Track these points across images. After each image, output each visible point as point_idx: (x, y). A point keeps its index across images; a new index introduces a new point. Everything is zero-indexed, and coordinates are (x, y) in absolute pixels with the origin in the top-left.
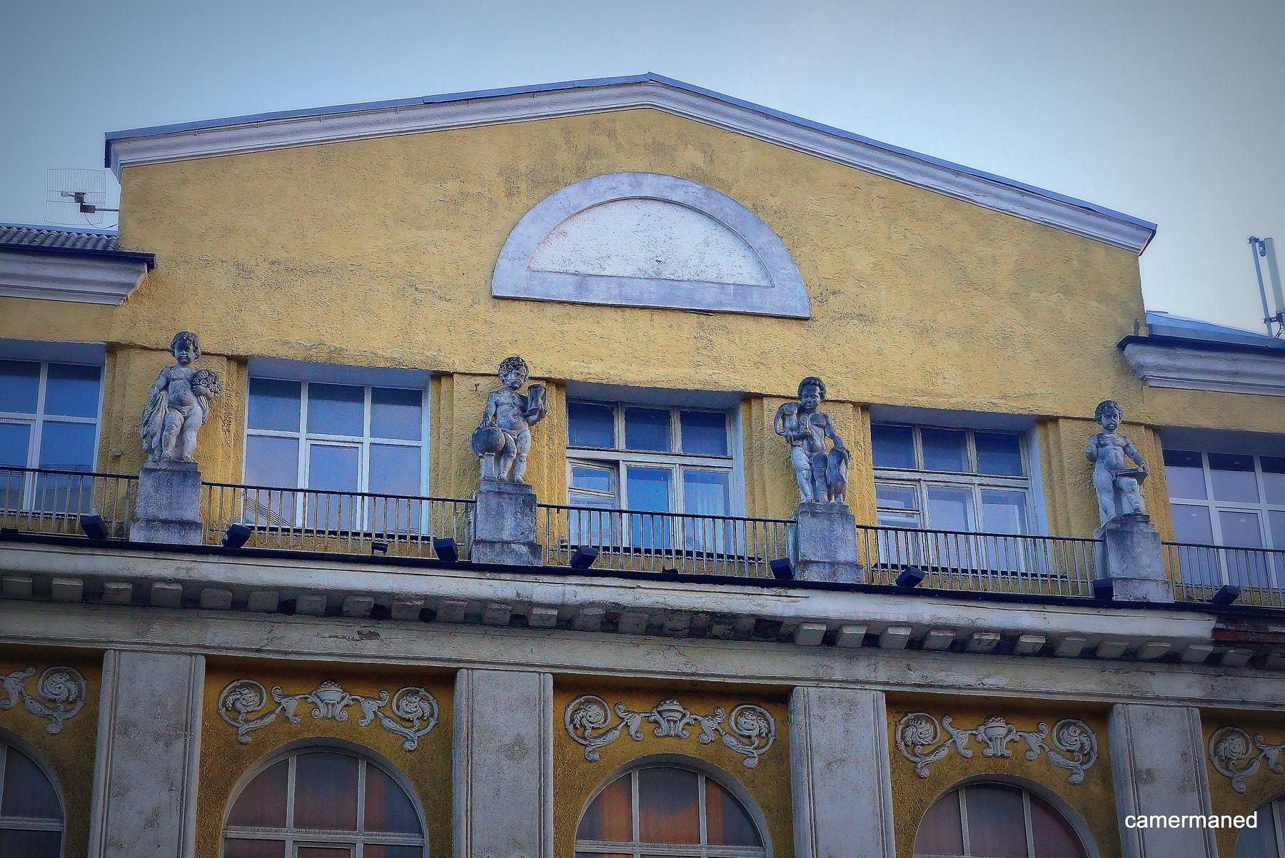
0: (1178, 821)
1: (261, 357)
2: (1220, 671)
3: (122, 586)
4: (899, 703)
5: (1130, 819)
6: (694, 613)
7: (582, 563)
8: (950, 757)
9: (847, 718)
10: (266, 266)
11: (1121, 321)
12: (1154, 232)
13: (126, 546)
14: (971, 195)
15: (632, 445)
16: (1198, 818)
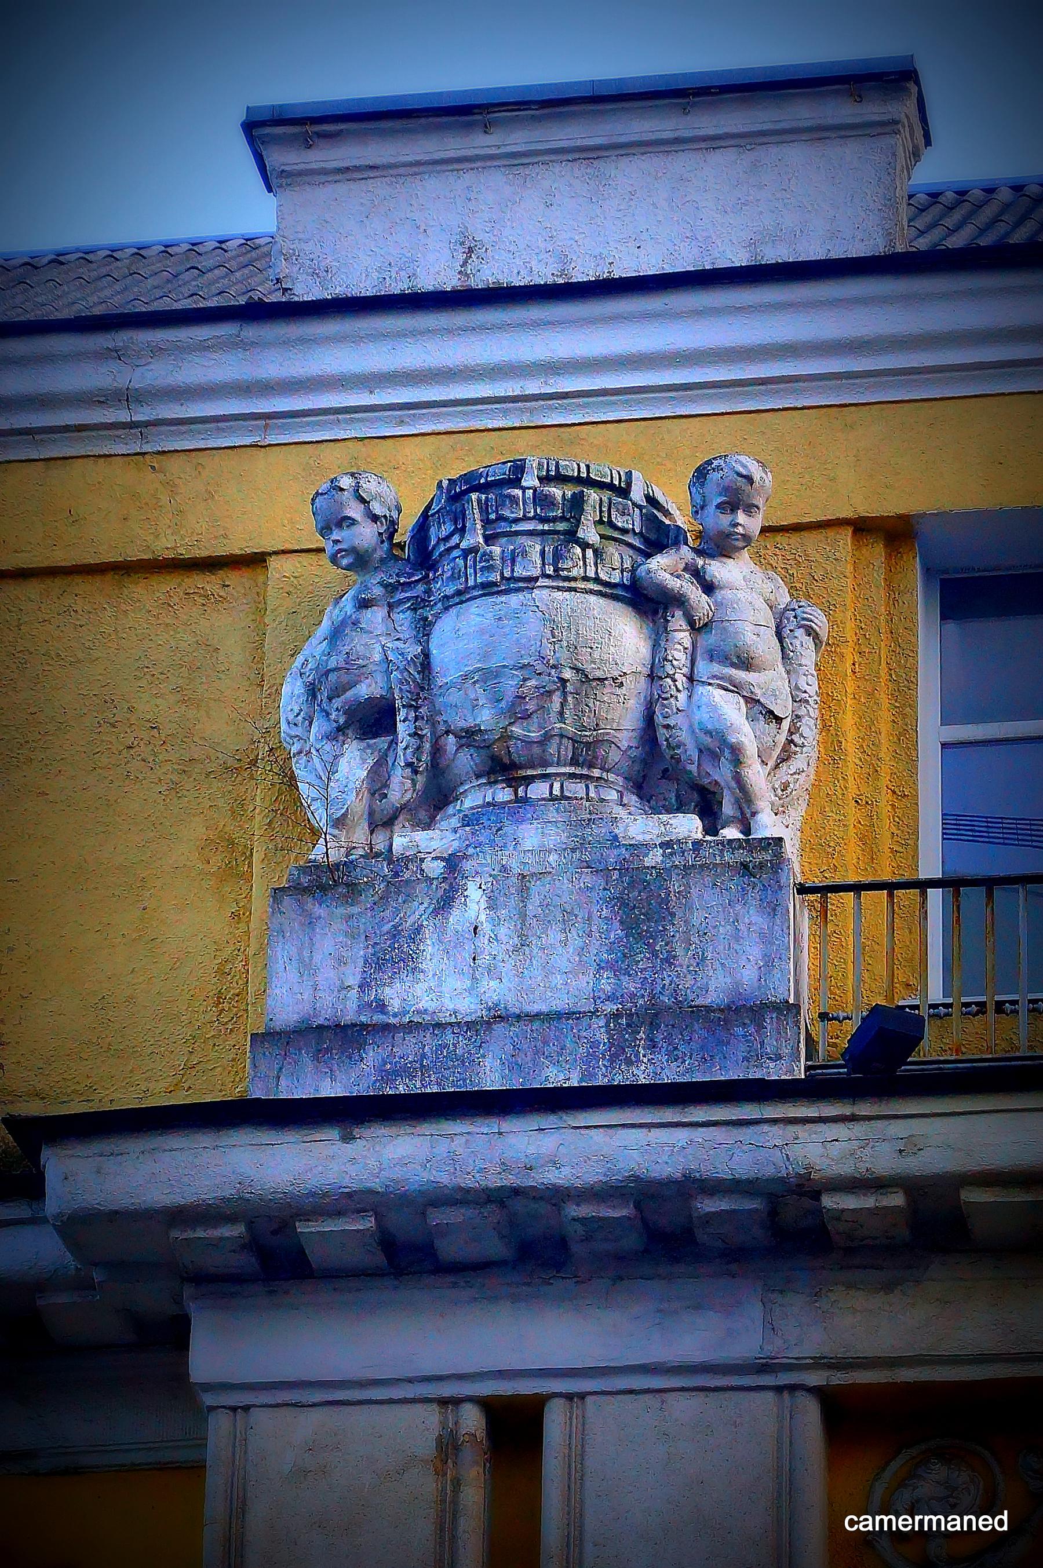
0: (910, 1522)
5: (851, 1520)
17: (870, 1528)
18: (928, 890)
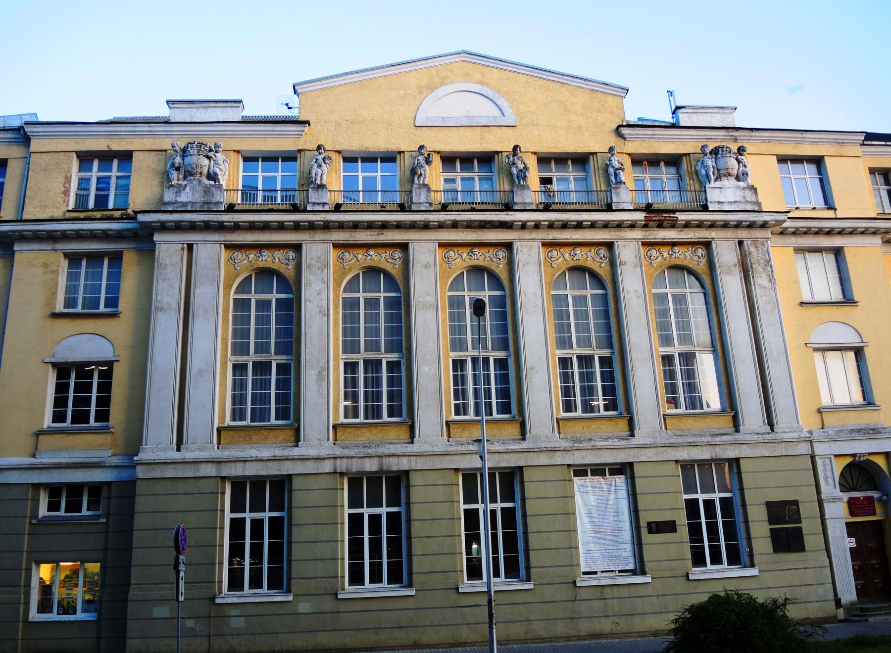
1: (345, 150)
2: (648, 229)
3: (305, 224)
4: (548, 245)
6: (480, 221)
7: (444, 208)
8: (562, 261)
9: (529, 251)
10: (344, 122)
11: (617, 120)
12: (628, 90)
13: (305, 211)
14: (569, 82)
15: (462, 170)
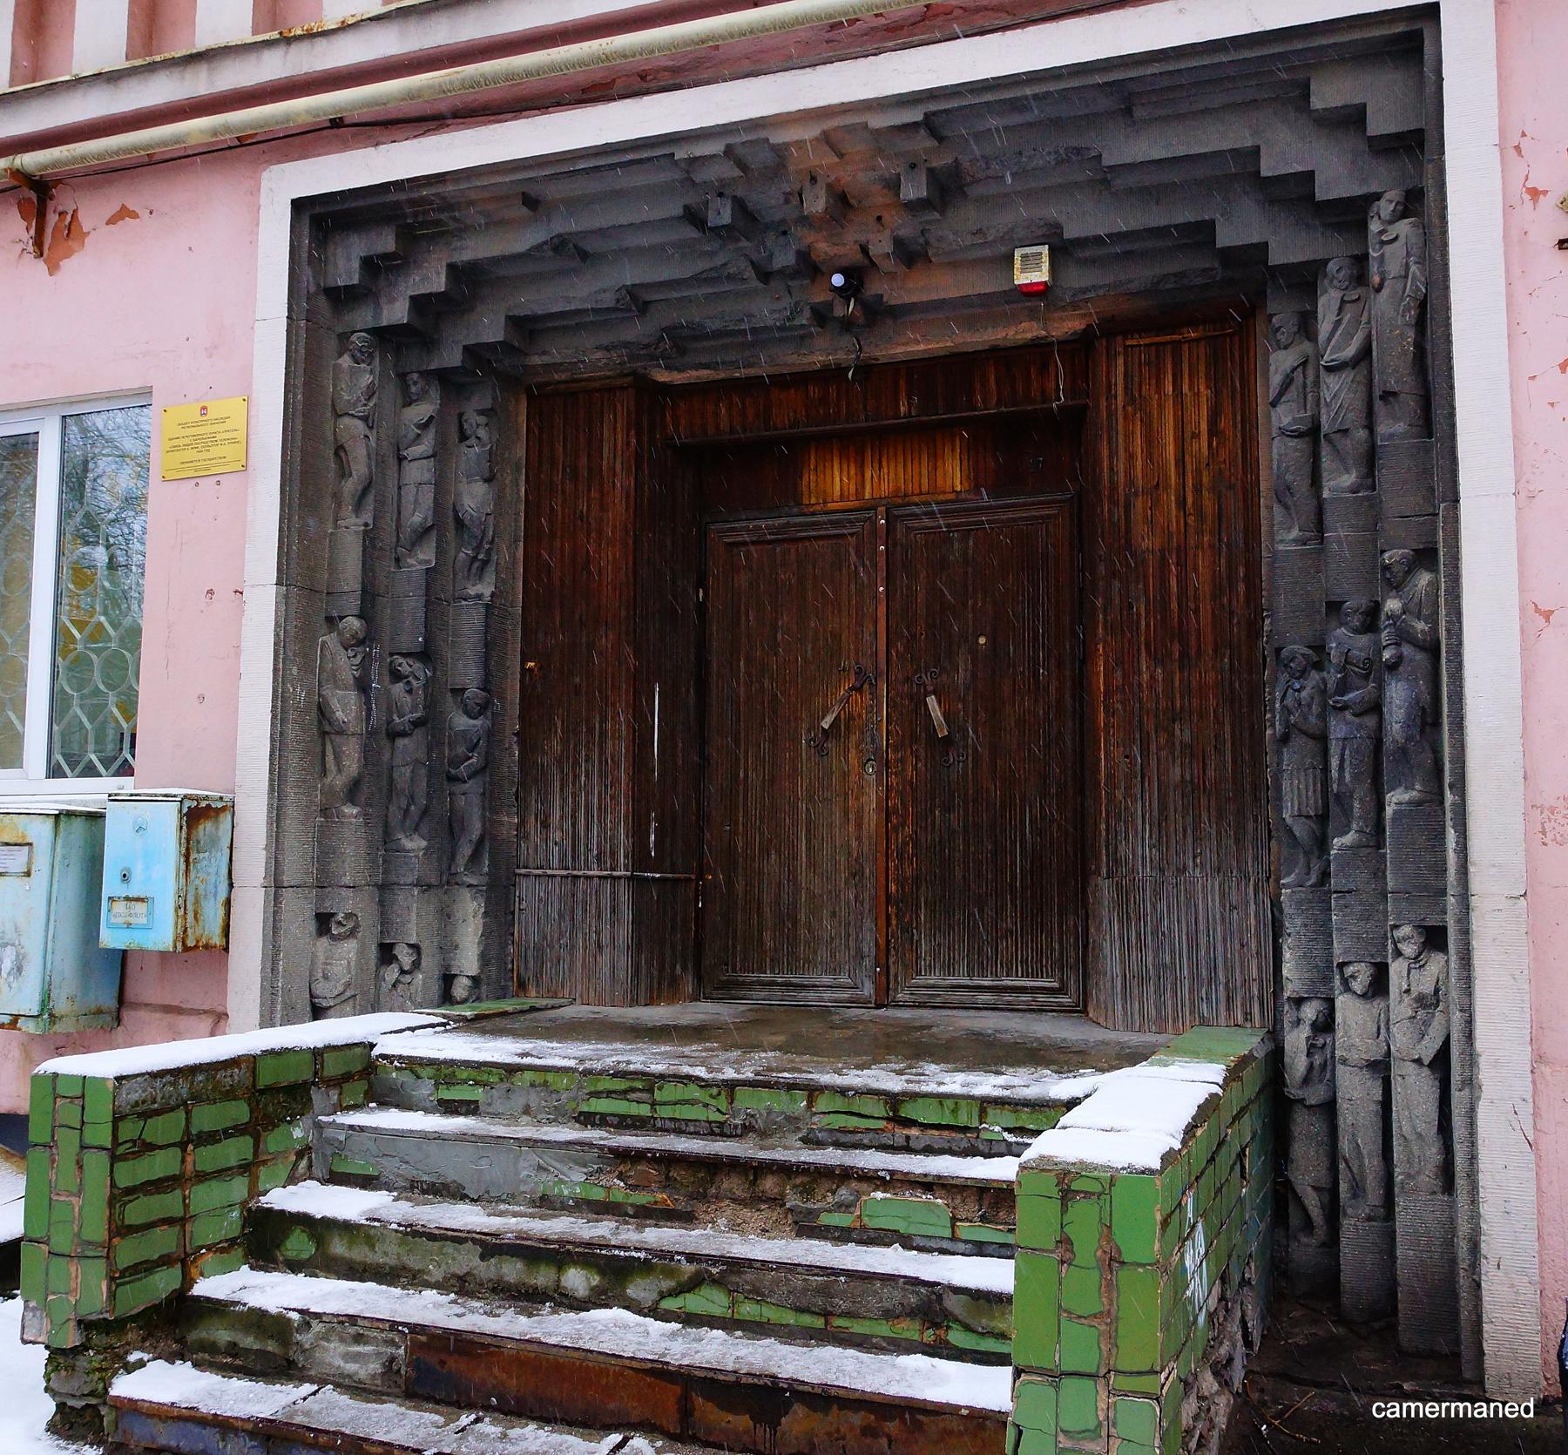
0: (1437, 1409)
1: (937, 5)
16: (1413, 1406)
17: (1397, 1415)
18: (101, 946)
